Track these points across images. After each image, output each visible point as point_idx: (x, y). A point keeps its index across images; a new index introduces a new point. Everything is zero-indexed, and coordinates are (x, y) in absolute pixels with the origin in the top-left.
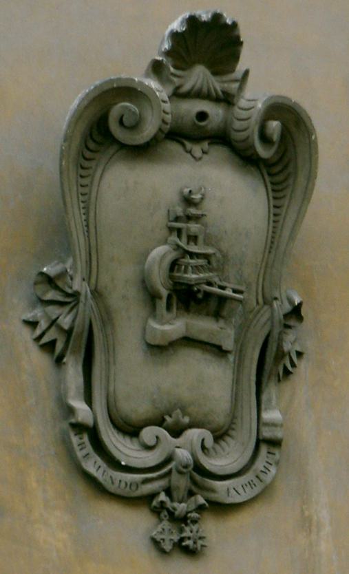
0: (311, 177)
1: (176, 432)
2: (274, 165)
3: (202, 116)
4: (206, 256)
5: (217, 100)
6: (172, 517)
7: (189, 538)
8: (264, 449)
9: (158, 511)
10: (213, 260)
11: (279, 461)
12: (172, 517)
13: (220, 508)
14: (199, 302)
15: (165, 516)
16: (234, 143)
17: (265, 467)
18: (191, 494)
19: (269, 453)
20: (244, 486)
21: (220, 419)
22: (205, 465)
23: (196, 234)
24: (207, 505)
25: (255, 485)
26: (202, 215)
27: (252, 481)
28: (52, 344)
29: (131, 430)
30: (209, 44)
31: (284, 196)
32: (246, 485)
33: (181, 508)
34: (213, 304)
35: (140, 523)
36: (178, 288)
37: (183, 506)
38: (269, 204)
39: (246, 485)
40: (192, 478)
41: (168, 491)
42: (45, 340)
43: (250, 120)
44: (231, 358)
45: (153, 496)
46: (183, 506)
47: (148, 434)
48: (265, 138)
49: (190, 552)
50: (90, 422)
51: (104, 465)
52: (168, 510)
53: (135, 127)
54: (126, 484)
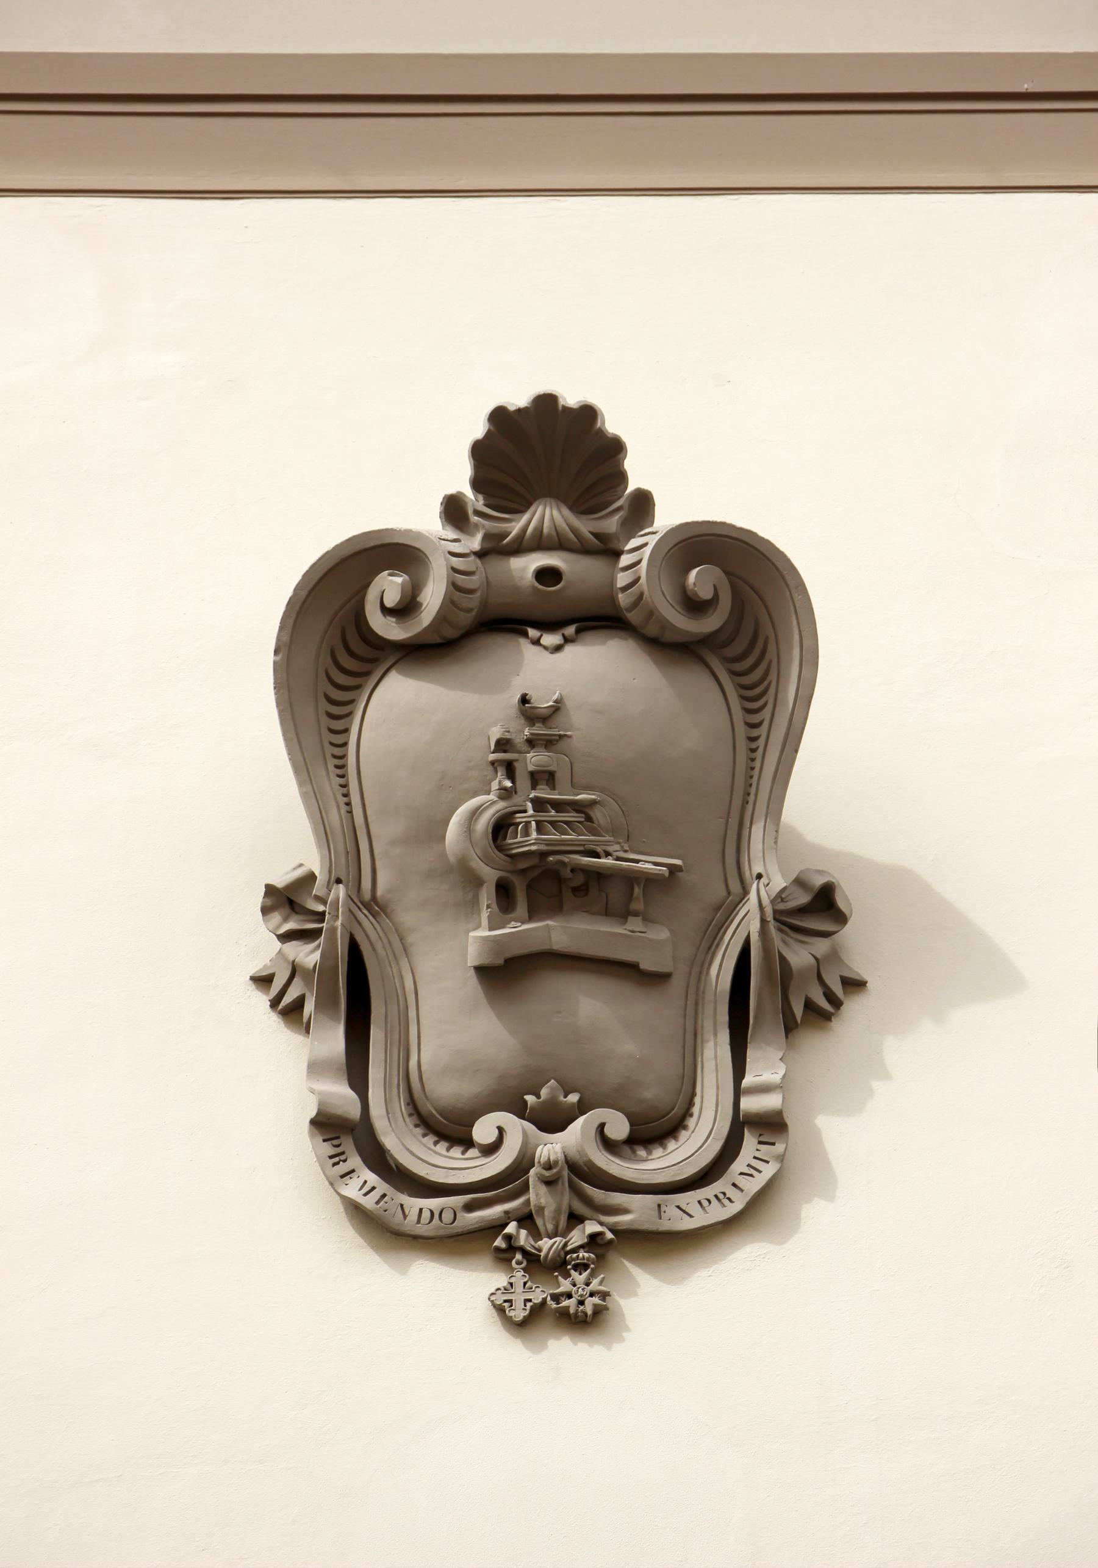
1: (552, 1121)
3: (547, 575)
4: (578, 807)
6: (533, 1261)
7: (569, 1296)
9: (504, 1256)
10: (597, 814)
11: (784, 1155)
13: (660, 1245)
14: (580, 891)
15: (519, 1263)
16: (398, 656)
17: (749, 1165)
18: (575, 1219)
21: (653, 1092)
24: (609, 1235)
25: (729, 1199)
26: (561, 737)
27: (724, 1194)
28: (298, 1005)
29: (452, 1129)
31: (765, 692)
32: (709, 1201)
34: (615, 893)
35: (474, 1285)
38: (321, 741)
39: (709, 1201)
40: (573, 1187)
41: (526, 1219)
42: (287, 999)
44: (676, 986)
45: (497, 1227)
47: (483, 1131)
49: (587, 1321)
51: (382, 1187)
52: (525, 1252)
53: (406, 609)
54: (432, 1212)
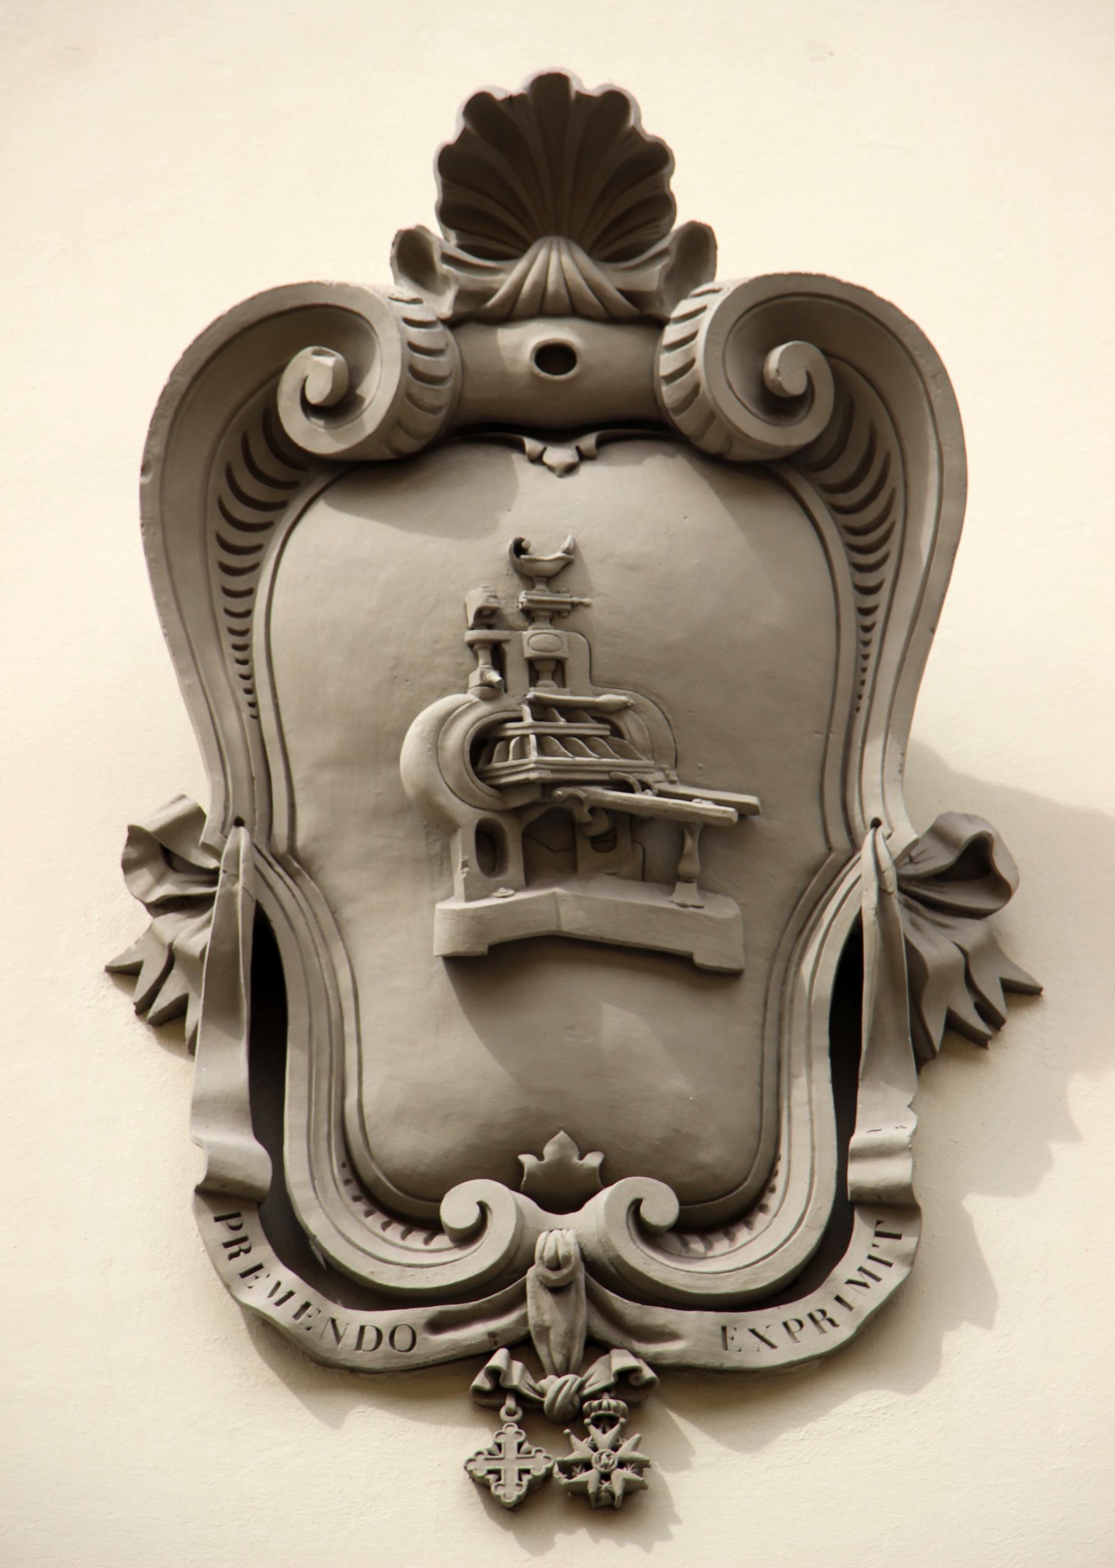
0: (342, 288)
2: (827, 463)
3: (554, 357)
4: (599, 713)
5: (610, 317)
6: (532, 1412)
8: (862, 1233)
9: (488, 1403)
10: (629, 724)
12: (532, 1412)
13: (725, 1389)
14: (604, 843)
15: (510, 1413)
17: (861, 1269)
18: (596, 1348)
19: (878, 1234)
20: (794, 1326)
22: (651, 1274)
23: (559, 654)
24: (648, 1373)
26: (574, 605)
27: (823, 1313)
28: (178, 1010)
29: (411, 1206)
30: (552, 169)
33: (554, 1387)
34: (657, 847)
36: (517, 801)
37: (577, 1381)
40: (593, 1298)
41: (522, 1346)
42: (162, 1002)
43: (692, 343)
44: (750, 990)
45: (477, 1357)
46: (577, 1381)
47: (457, 1208)
48: (777, 404)
49: (613, 1506)
50: (261, 1174)
51: (304, 1292)
53: (339, 406)
